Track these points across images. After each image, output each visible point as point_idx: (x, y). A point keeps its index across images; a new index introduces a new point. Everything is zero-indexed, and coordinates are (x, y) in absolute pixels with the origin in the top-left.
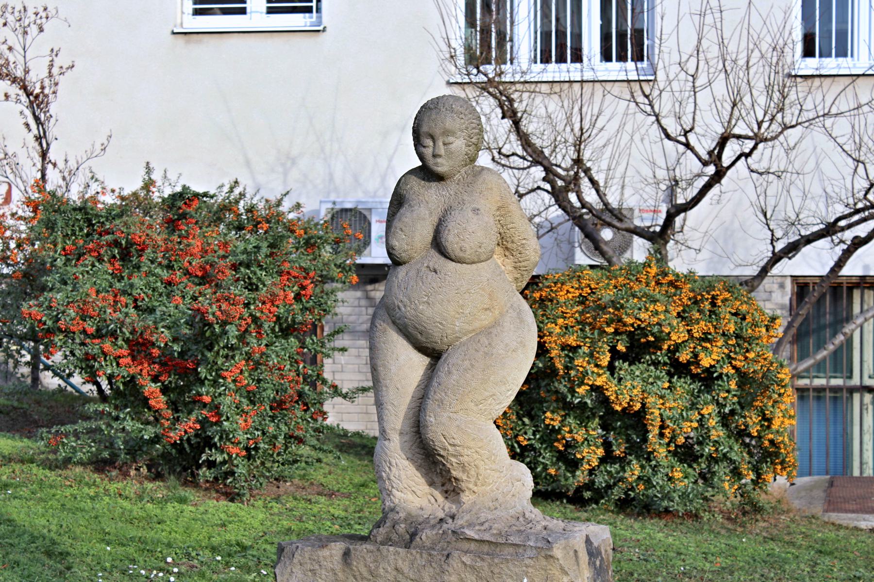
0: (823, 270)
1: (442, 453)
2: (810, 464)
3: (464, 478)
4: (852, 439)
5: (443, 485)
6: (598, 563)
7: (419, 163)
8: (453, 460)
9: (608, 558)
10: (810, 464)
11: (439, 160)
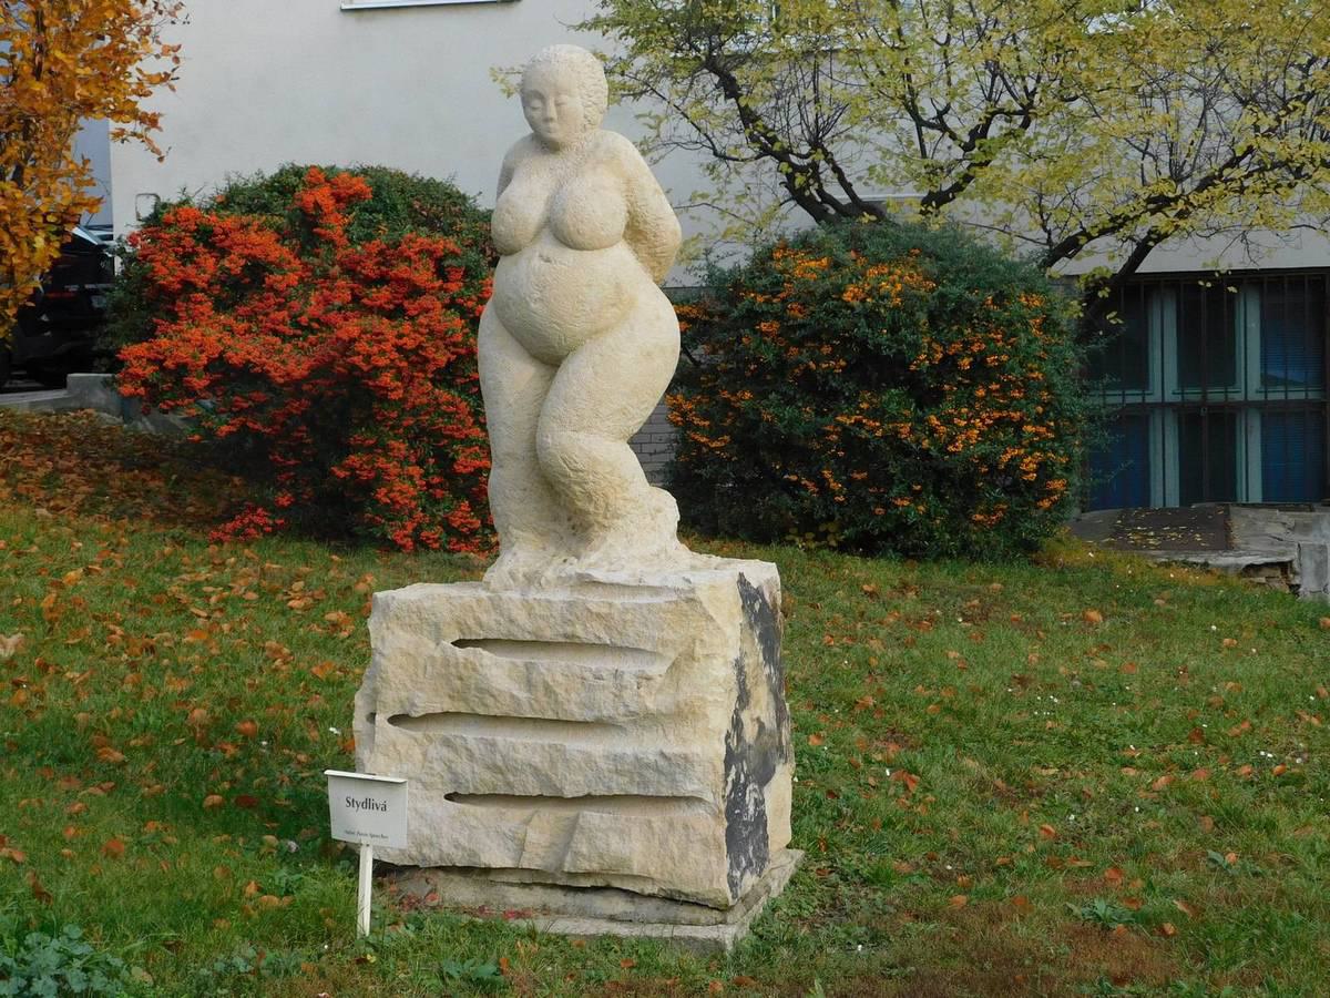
0: (1117, 265)
1: (563, 480)
2: (523, 720)
3: (592, 509)
4: (1238, 453)
5: (569, 519)
6: (757, 607)
7: (530, 131)
8: (577, 488)
9: (775, 599)
10: (523, 720)
11: (551, 125)
